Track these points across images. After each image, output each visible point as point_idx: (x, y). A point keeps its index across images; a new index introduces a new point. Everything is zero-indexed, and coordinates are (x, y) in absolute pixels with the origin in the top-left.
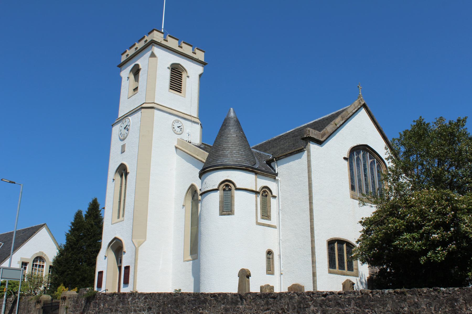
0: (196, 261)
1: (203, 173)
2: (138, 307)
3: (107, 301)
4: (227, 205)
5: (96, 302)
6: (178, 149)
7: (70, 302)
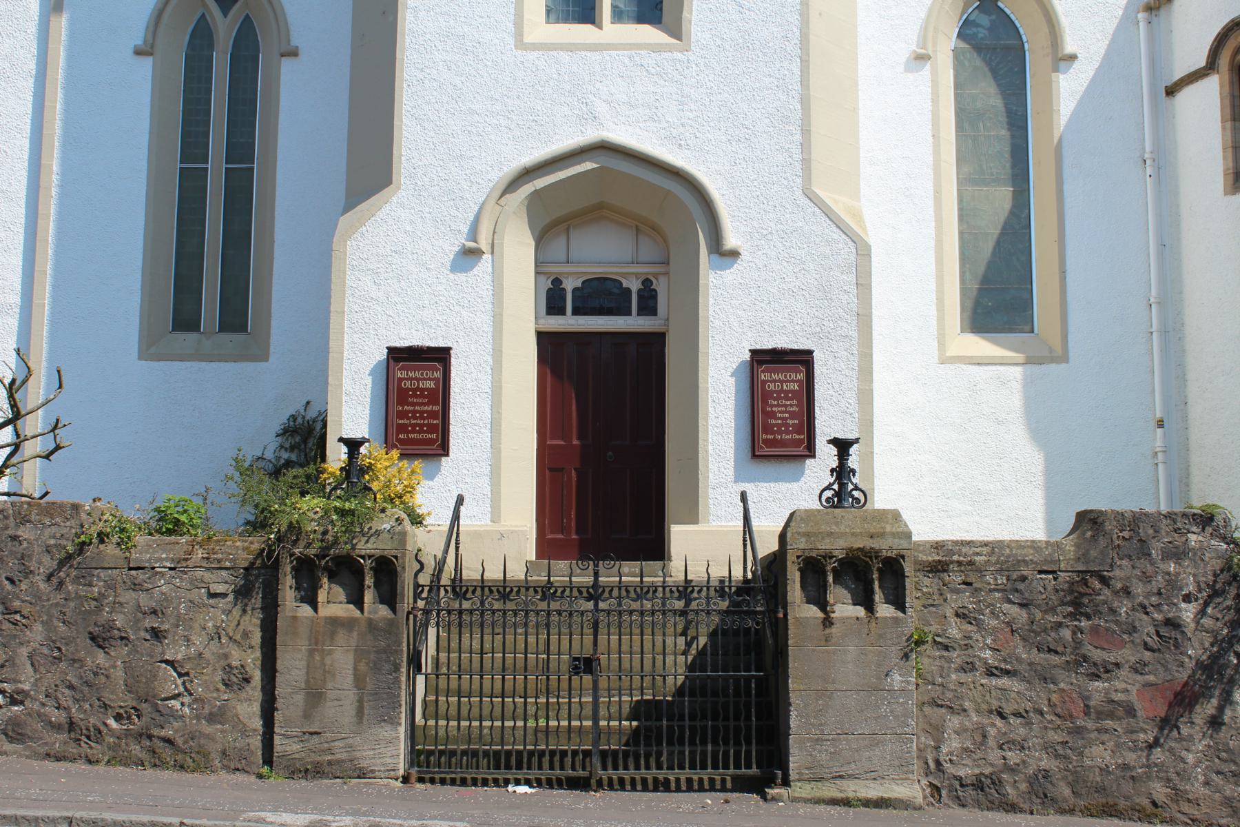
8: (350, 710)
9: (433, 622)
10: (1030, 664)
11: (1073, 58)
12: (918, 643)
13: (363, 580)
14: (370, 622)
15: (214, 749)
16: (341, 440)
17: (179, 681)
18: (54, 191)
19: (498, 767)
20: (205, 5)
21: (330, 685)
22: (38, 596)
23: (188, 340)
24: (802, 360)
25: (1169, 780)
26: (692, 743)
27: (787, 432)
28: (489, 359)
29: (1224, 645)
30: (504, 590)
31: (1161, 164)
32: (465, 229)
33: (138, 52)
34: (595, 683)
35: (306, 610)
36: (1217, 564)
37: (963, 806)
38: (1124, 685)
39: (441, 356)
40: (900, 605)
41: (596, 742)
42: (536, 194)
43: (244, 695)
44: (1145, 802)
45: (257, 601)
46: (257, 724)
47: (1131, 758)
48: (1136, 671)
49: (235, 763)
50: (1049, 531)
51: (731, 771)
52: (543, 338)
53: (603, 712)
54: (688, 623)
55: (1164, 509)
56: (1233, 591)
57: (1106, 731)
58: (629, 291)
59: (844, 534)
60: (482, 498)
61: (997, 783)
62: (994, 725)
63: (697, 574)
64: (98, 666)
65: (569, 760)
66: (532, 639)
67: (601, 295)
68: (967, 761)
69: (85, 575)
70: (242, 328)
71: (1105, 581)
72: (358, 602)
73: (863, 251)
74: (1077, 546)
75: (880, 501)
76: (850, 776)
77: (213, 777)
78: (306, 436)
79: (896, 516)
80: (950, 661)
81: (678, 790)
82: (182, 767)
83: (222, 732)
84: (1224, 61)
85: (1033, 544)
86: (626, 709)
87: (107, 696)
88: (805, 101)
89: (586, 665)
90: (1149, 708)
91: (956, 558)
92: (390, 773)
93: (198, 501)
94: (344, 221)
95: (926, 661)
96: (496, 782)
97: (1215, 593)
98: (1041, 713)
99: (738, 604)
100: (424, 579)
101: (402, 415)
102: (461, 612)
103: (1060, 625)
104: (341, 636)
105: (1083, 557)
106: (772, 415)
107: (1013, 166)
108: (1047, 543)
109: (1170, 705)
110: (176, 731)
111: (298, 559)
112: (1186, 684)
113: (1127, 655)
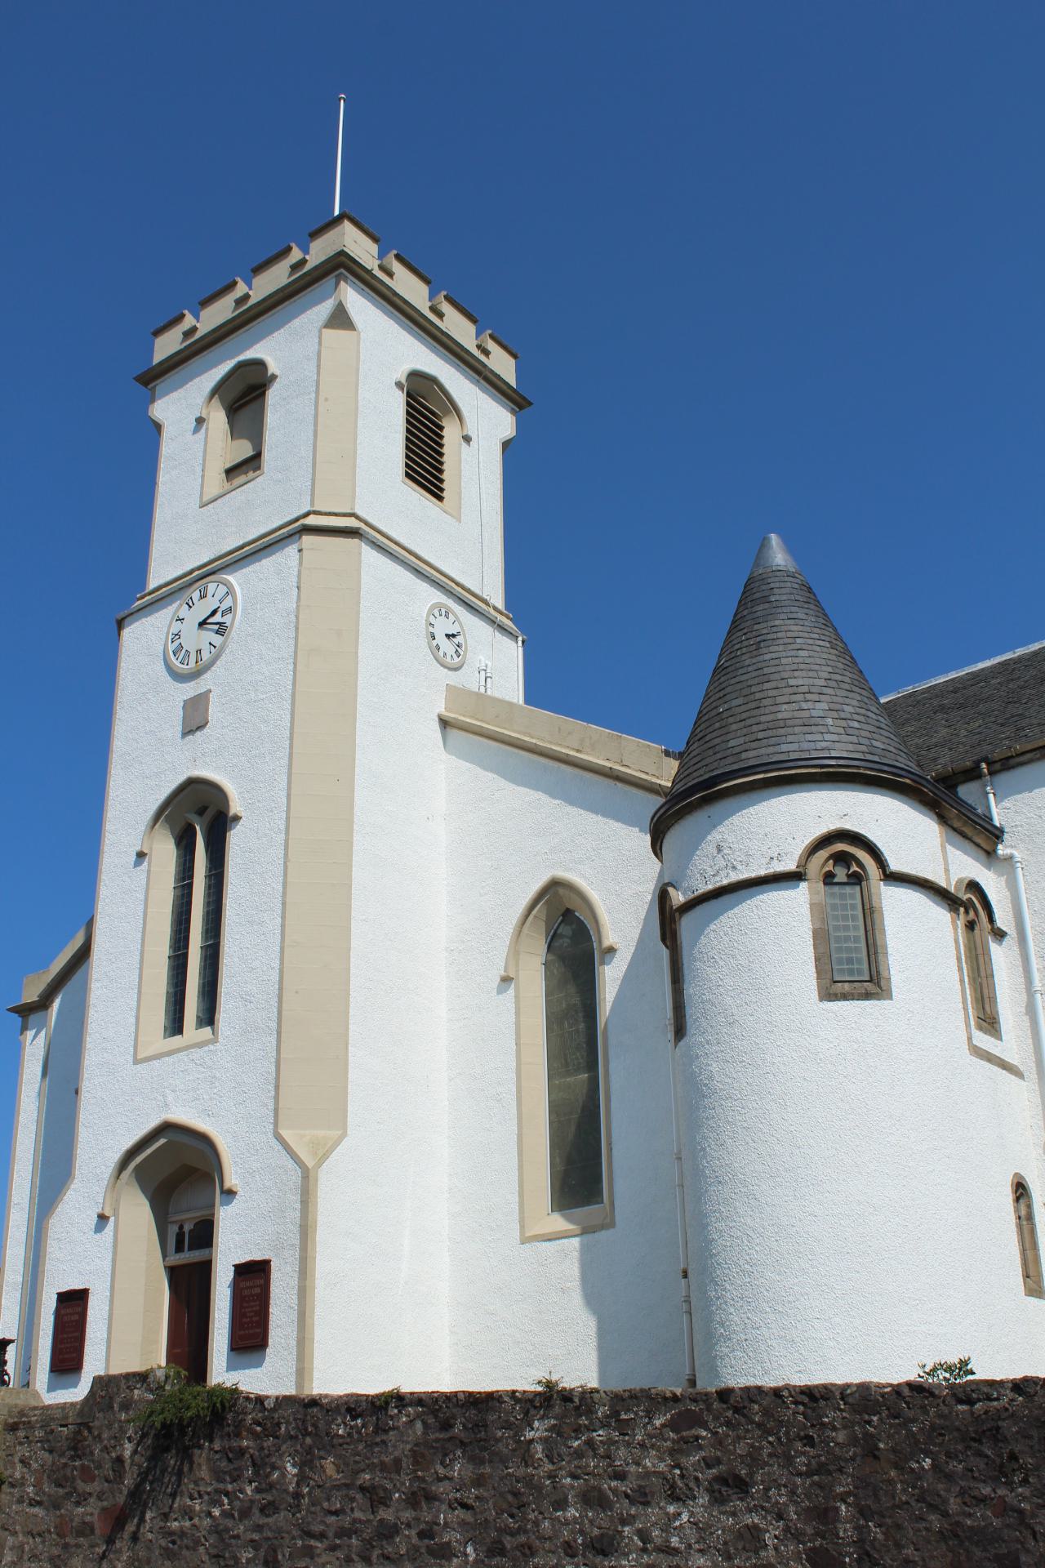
0: (603, 1235)
1: (676, 811)
2: (620, 1476)
3: (330, 1444)
4: (849, 950)
5: (242, 1452)
6: (453, 733)
7: (23, 1451)
103: (65, 1465)
113: (95, 1487)
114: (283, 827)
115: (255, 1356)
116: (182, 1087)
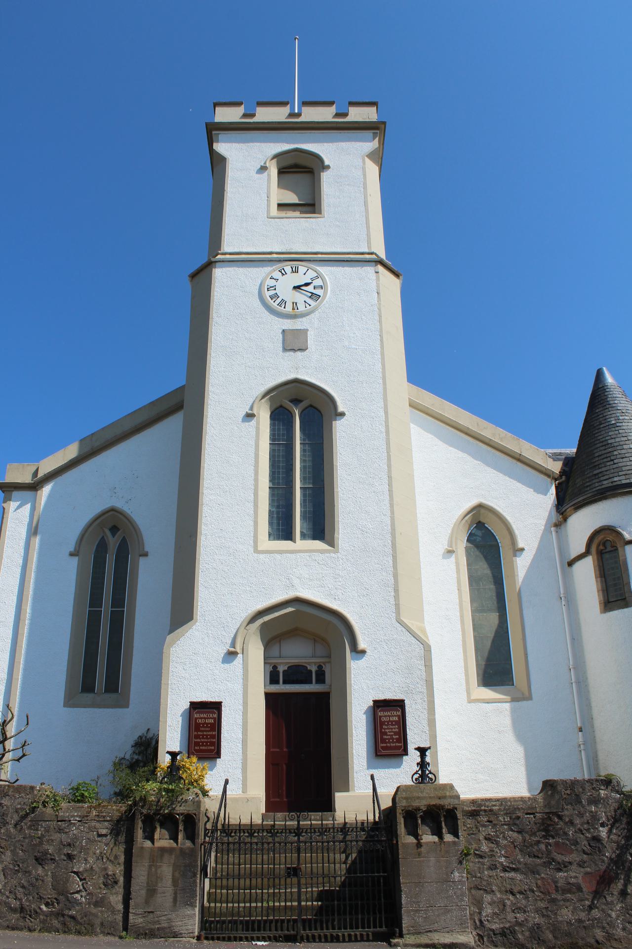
8: (170, 899)
9: (214, 849)
10: (525, 864)
11: (522, 550)
12: (467, 855)
13: (178, 827)
14: (181, 849)
15: (97, 922)
16: (168, 752)
17: (80, 883)
18: (27, 622)
19: (247, 930)
20: (104, 532)
21: (160, 885)
22: (9, 836)
23: (89, 696)
24: (399, 705)
25: (604, 928)
26: (350, 914)
27: (393, 742)
28: (241, 707)
29: (623, 849)
30: (250, 830)
31: (569, 599)
32: (229, 641)
33: (72, 554)
34: (299, 882)
35: (148, 844)
36: (616, 805)
37: (496, 946)
38: (574, 874)
39: (217, 706)
40: (456, 835)
41: (300, 915)
42: (264, 624)
43: (114, 891)
44: (593, 941)
45: (122, 838)
46: (120, 907)
47: (583, 915)
48: (580, 866)
49: (108, 930)
50: (530, 790)
51: (372, 929)
52: (268, 696)
53: (303, 897)
54: (346, 846)
55: (586, 777)
56: (624, 820)
57: (568, 900)
58: (311, 671)
59: (425, 797)
60: (237, 781)
61: (513, 932)
62: (509, 899)
63: (350, 818)
64: (38, 875)
65: (285, 925)
66: (265, 857)
67: (297, 674)
68: (497, 920)
69: (34, 825)
70: (116, 690)
71: (560, 817)
72: (175, 838)
73: (427, 649)
74: (544, 799)
75: (443, 779)
76: (435, 931)
77: (95, 938)
78: (147, 747)
79: (451, 787)
80: (483, 864)
81: (344, 941)
82: (79, 932)
83: (102, 912)
84: (594, 549)
85: (522, 799)
86: (315, 895)
87: (42, 892)
88: (395, 576)
89: (294, 872)
90: (587, 888)
91: (483, 808)
92: (190, 934)
93: (93, 784)
94: (169, 638)
95: (471, 864)
96: (247, 939)
97: (616, 820)
98: (533, 891)
99: (372, 837)
100: (209, 826)
101: (197, 737)
102: (228, 843)
103: (538, 842)
104: (166, 856)
105: (547, 805)
106: (386, 734)
107: (498, 603)
108: (529, 798)
109: (598, 883)
110: (77, 912)
111: (145, 815)
112: (605, 871)
113: (575, 857)
114: (383, 430)
115: (393, 761)
116: (307, 576)
